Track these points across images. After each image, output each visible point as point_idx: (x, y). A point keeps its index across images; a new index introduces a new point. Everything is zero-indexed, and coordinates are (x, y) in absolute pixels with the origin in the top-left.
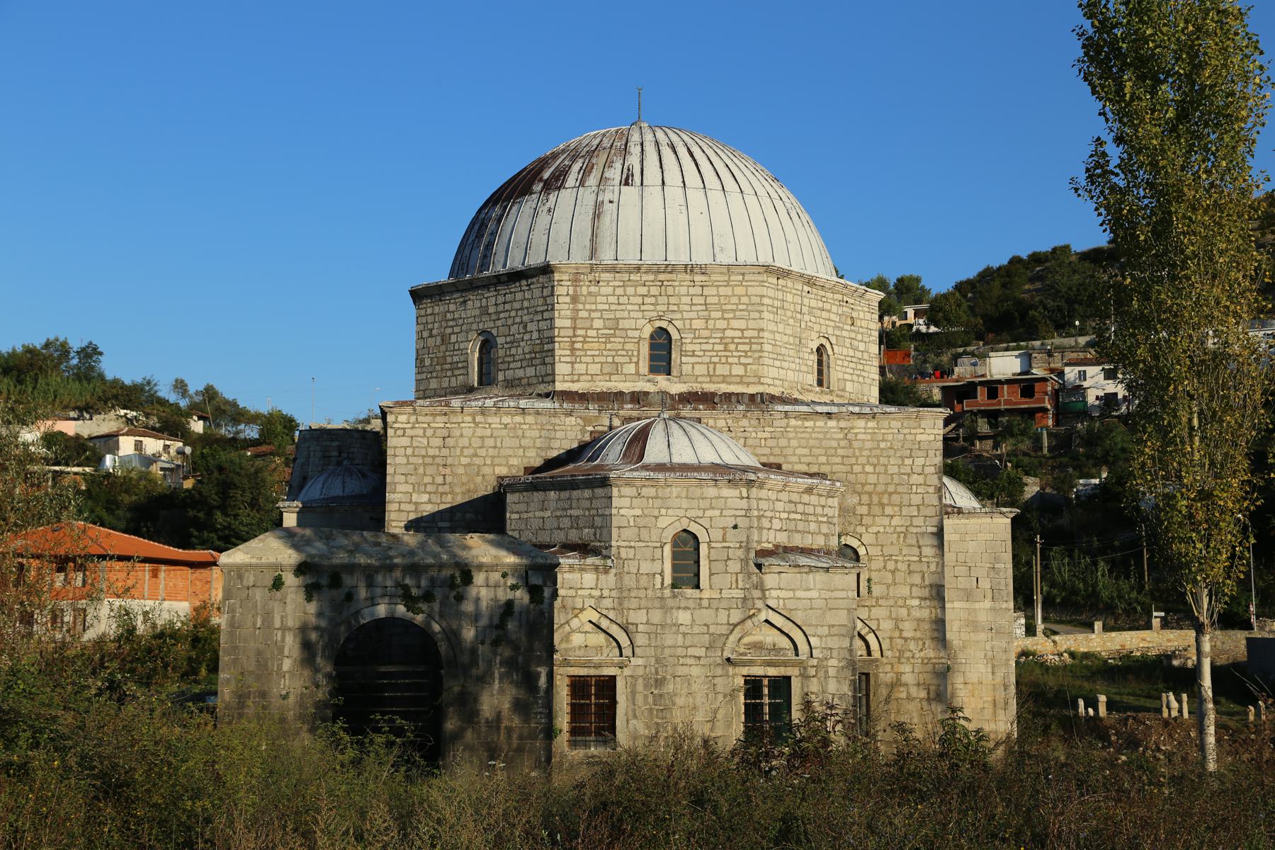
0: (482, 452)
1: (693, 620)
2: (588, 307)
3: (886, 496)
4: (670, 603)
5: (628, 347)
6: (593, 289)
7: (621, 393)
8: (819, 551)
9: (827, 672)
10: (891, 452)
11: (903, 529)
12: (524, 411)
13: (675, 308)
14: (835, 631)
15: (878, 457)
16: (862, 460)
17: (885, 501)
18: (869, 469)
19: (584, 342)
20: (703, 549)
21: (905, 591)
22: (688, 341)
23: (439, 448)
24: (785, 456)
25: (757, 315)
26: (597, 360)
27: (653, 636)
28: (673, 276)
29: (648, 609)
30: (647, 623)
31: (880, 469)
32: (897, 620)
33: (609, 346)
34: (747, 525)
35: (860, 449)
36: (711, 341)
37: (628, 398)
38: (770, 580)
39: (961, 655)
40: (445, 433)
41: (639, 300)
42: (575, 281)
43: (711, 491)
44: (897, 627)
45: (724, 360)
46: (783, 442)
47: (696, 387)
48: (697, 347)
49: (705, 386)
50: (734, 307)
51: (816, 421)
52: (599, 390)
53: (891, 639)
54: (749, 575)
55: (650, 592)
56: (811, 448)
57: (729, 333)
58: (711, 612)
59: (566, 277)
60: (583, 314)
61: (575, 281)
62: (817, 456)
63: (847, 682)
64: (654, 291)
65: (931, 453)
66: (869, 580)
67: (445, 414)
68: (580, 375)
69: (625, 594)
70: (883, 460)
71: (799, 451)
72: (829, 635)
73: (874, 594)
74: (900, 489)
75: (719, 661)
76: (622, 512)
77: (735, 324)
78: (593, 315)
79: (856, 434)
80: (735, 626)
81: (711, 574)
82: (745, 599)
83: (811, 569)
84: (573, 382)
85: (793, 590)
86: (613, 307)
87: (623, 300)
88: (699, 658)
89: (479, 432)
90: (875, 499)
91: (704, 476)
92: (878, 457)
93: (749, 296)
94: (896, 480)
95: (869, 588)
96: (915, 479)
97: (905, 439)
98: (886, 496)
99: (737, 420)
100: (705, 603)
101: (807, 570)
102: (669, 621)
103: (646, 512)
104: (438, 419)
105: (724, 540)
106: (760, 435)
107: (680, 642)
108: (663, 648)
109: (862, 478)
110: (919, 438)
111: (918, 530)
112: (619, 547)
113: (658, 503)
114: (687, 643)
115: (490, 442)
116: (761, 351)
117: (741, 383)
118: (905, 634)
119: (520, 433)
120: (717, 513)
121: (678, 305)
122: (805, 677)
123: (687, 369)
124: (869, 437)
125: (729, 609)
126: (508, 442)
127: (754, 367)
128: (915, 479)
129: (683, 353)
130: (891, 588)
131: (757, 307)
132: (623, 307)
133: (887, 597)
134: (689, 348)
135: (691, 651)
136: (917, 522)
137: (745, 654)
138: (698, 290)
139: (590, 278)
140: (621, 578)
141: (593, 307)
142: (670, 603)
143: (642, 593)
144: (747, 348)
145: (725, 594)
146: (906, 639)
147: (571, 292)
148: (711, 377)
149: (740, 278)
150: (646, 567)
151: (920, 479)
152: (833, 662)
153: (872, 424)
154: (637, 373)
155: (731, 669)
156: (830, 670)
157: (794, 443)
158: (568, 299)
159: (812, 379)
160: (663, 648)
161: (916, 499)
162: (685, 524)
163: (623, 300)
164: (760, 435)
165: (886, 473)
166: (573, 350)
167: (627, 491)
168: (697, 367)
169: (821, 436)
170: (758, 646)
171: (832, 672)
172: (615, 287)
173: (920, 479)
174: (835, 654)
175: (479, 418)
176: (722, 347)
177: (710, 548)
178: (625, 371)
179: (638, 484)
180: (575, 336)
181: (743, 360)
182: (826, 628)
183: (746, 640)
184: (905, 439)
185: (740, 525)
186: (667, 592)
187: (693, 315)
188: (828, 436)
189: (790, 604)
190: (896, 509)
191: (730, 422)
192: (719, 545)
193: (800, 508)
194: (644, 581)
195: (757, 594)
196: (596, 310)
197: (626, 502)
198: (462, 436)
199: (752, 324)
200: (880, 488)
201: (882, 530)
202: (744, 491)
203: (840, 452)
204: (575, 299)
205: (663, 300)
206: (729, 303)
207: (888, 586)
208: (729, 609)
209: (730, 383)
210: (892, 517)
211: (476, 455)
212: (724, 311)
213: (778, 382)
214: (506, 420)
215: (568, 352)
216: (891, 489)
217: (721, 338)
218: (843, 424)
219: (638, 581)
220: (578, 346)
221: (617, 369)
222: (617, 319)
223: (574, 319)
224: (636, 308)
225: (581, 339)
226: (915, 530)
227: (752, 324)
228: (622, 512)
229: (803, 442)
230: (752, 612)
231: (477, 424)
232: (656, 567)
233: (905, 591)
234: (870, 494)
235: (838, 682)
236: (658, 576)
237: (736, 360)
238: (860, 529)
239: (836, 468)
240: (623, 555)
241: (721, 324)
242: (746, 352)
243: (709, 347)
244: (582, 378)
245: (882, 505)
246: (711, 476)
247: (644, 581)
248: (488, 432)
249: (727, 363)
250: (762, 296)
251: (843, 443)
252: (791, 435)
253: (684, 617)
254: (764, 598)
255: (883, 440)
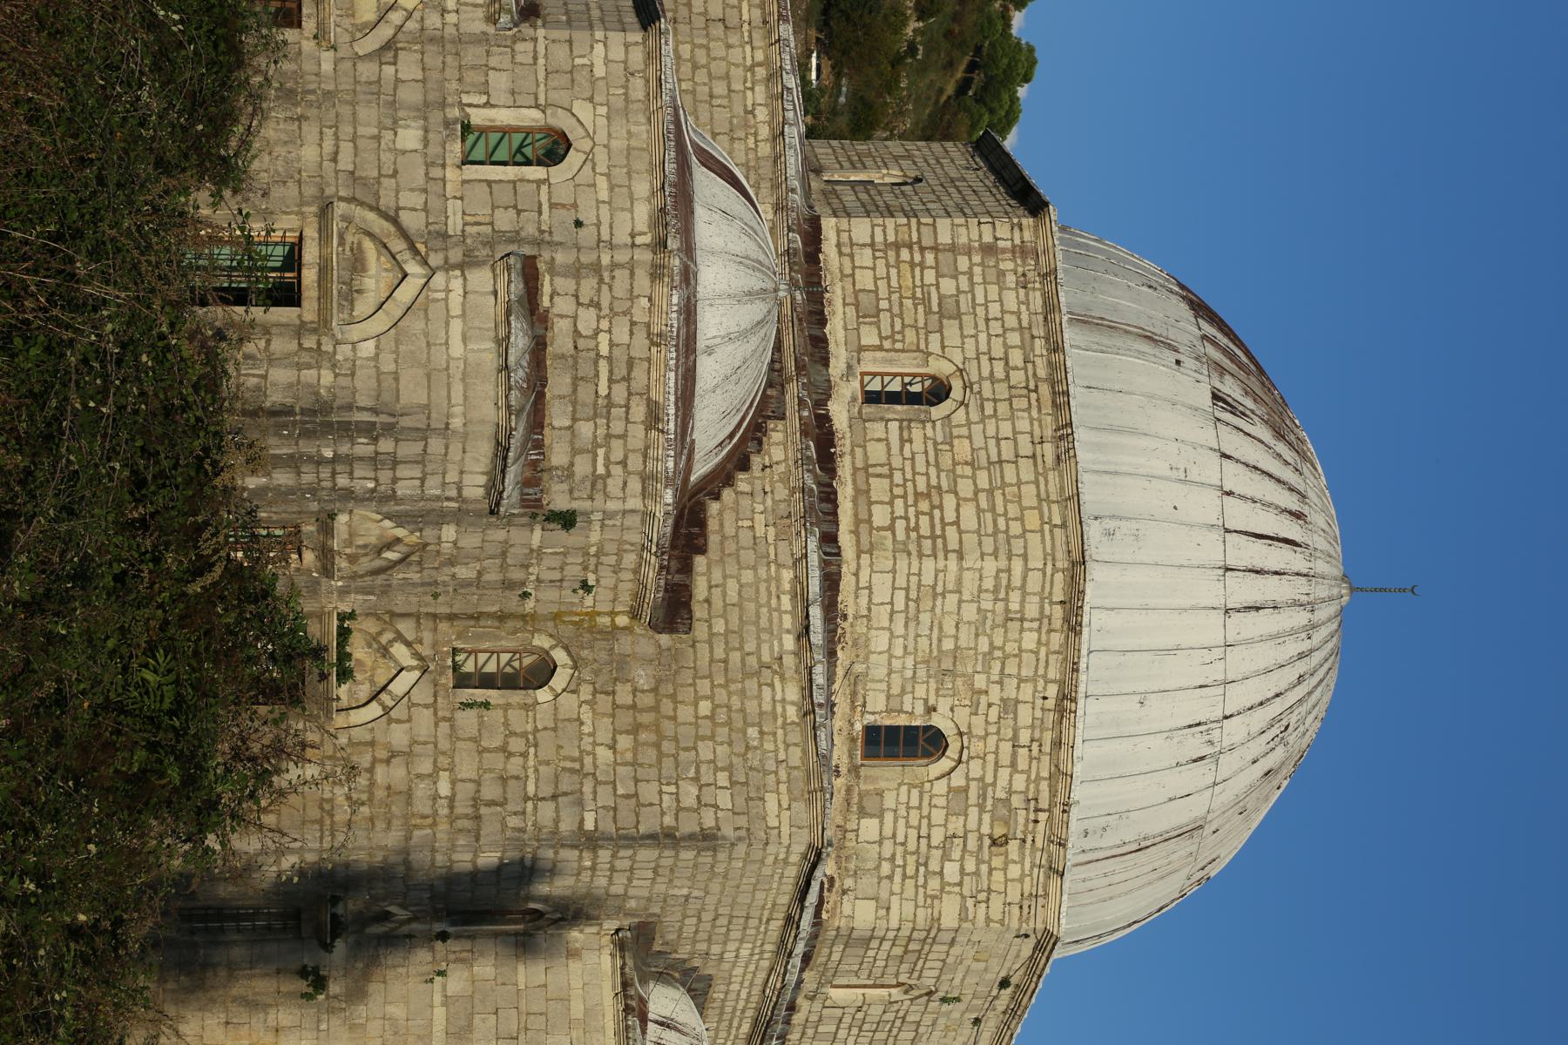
0: (702, 76)
1: (404, 152)
2: (977, 270)
3: (653, 737)
4: (436, 117)
5: (910, 335)
6: (1011, 279)
7: (823, 322)
8: (539, 445)
9: (309, 367)
10: (740, 749)
11: (588, 767)
12: (778, 136)
13: (989, 410)
14: (388, 382)
15: (729, 723)
16: (721, 695)
17: (643, 736)
18: (705, 707)
19: (912, 265)
20: (535, 172)
21: (467, 769)
22: (930, 433)
23: (706, 13)
24: (722, 560)
25: (989, 548)
26: (882, 284)
27: (374, 88)
28: (1047, 408)
29: (424, 81)
30: (398, 81)
31: (705, 729)
32: (409, 755)
33: (908, 303)
34: (582, 242)
35: (743, 692)
36: (933, 471)
37: (816, 332)
38: (481, 278)
39: (336, 1021)
40: (733, 20)
41: (998, 352)
42: (1022, 251)
43: (642, 187)
44: (393, 754)
45: (898, 491)
46: (748, 556)
47: (843, 444)
48: (918, 446)
49: (847, 460)
50: (1000, 510)
51: (793, 613)
52: (826, 283)
53: (372, 743)
54: (490, 244)
55: (454, 85)
56: (740, 605)
57: (949, 502)
58: (420, 180)
59: (1028, 236)
60: (963, 263)
61: (1022, 251)
62: (724, 616)
63: (289, 401)
64: (1017, 377)
65: (742, 821)
66: (486, 705)
67: (765, 22)
68: (852, 256)
69: (448, 46)
70: (722, 733)
71: (732, 586)
72: (379, 373)
73: (460, 715)
74: (668, 763)
75: (329, 191)
76: (599, 48)
77: (968, 511)
78: (963, 280)
79: (772, 685)
80: (395, 221)
81: (489, 183)
82: (445, 236)
83: (503, 343)
84: (839, 245)
85: (463, 315)
86: (980, 311)
87: (996, 327)
88: (335, 160)
89: (737, 73)
90: (646, 718)
91: (670, 167)
92: (729, 723)
93: (1023, 535)
94: (683, 756)
95: (470, 706)
96: (690, 793)
97: (766, 773)
98: (653, 737)
99: (785, 479)
100: (436, 172)
101: (502, 333)
102: (401, 114)
103: (601, 83)
104: (757, 13)
105: (552, 206)
106: (760, 520)
107: (361, 131)
108: (353, 104)
109: (686, 694)
110: (771, 799)
111: (588, 795)
112: (535, 40)
113: (619, 103)
114: (361, 143)
115: (720, 88)
116: (921, 556)
117: (857, 521)
118: (380, 771)
119: (740, 134)
120: (604, 195)
121: (995, 415)
122: (300, 330)
123: (877, 430)
124: (767, 707)
125: (426, 210)
126: (721, 116)
127: (889, 543)
128: (690, 793)
129: (906, 425)
130: (472, 745)
131: (1004, 545)
132: (982, 326)
133: (453, 736)
134: (917, 433)
135: (346, 149)
136: (605, 797)
137: (342, 242)
138: (1025, 448)
139: (1030, 275)
140: (479, 42)
141: (978, 279)
142: (436, 117)
143: (451, 73)
144: (925, 529)
145: (454, 207)
146: (371, 770)
147: (1001, 244)
148: (865, 471)
149: (1057, 520)
150: (500, 82)
151: (689, 800)
152: (327, 377)
153: (792, 712)
154: (861, 349)
155: (313, 209)
156: (313, 372)
157: (748, 576)
158: (988, 238)
159: (878, 711)
160: (353, 104)
161: (648, 792)
162: (580, 143)
163: (996, 327)
164: (760, 520)
165: (698, 738)
166: (897, 246)
167: (637, 57)
168: (882, 446)
169: (764, 622)
170: (357, 264)
171: (309, 375)
172: (1018, 314)
173: (689, 800)
174: (343, 381)
175: (761, 72)
176: (922, 487)
177: (539, 183)
178: (864, 329)
179: (651, 72)
180: (922, 249)
181: (900, 525)
182: (392, 367)
183: (368, 245)
184: (766, 773)
185: (583, 232)
186: (455, 113)
187: (979, 441)
188: (764, 636)
189: (436, 311)
190: (629, 756)
191: (782, 468)
192: (544, 198)
193: (619, 393)
194: (473, 77)
195: (456, 255)
196: (972, 284)
197: (617, 53)
198: (729, 46)
199: (970, 540)
200: (668, 727)
201: (586, 729)
202: (647, 239)
203: (735, 657)
204: (989, 250)
205: (1002, 391)
206: (1006, 501)
207: (476, 740)
208: (426, 210)
209: (855, 501)
210: (612, 747)
211: (695, 67)
212: (990, 492)
213: (863, 601)
214: (762, 114)
215: (891, 238)
216: (667, 746)
217: (939, 487)
218: (789, 661)
219: (473, 67)
220: (905, 254)
221: (867, 313)
222: (958, 316)
223: (953, 248)
224: (983, 347)
225: (917, 258)
226: (588, 788)
227: (970, 540)
228: (599, 48)
229: (749, 592)
230: (421, 248)
231: (751, 69)
232: (500, 96)
233: (467, 769)
234: (656, 708)
235: (290, 386)
236: (484, 99)
237: (900, 511)
238: (586, 692)
239: (703, 649)
240: (519, 47)
241: (965, 488)
242: (917, 529)
243: (920, 467)
244: (847, 261)
245: (635, 730)
246: (672, 178)
247: (473, 77)
248: (738, 86)
249: (894, 497)
250: (1025, 557)
251: (752, 661)
252: (762, 572)
253: (410, 137)
254: (448, 267)
255: (761, 733)
